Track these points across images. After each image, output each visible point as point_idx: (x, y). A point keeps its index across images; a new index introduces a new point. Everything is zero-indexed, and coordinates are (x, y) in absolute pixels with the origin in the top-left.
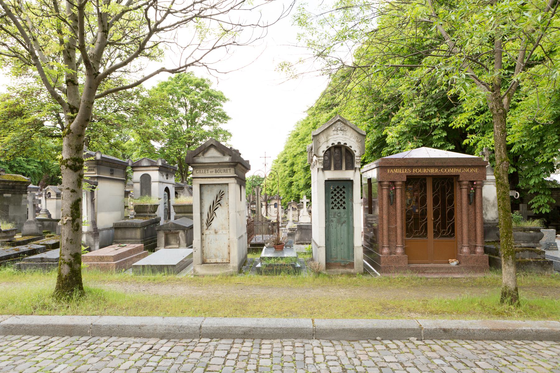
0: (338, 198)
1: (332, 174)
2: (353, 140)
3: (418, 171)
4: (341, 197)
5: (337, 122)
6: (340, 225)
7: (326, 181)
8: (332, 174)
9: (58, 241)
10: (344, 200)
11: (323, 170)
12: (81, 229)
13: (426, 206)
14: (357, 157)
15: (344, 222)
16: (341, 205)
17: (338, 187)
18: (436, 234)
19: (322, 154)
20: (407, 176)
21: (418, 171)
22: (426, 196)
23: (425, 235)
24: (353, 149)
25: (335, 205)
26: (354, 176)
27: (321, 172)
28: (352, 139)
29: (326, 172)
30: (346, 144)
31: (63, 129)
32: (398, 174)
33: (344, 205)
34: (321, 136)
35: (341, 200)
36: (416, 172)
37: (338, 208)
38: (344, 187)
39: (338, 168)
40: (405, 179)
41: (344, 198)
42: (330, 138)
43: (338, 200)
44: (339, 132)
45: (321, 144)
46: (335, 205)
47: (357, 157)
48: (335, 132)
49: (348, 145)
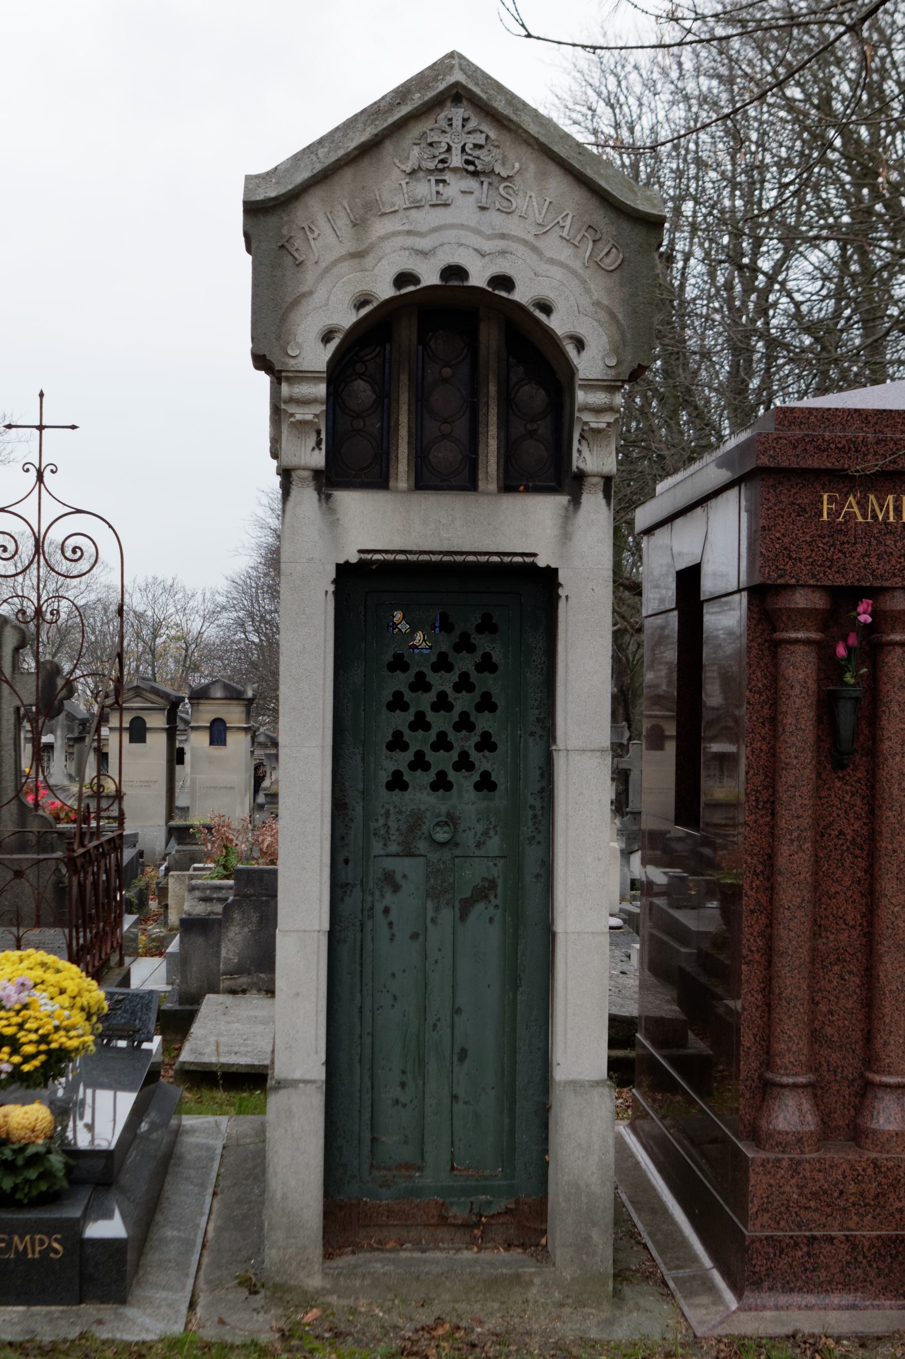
0: (442, 704)
1: (380, 523)
2: (565, 254)
4: (462, 702)
6: (447, 915)
10: (484, 722)
14: (591, 385)
15: (484, 892)
16: (464, 763)
28: (554, 247)
30: (404, 279)
33: (483, 762)
37: (441, 784)
38: (487, 626)
41: (487, 704)
42: (380, 227)
43: (440, 722)
44: (455, 185)
45: (310, 275)
46: (419, 763)
47: (591, 385)
48: (424, 189)
49: (522, 295)
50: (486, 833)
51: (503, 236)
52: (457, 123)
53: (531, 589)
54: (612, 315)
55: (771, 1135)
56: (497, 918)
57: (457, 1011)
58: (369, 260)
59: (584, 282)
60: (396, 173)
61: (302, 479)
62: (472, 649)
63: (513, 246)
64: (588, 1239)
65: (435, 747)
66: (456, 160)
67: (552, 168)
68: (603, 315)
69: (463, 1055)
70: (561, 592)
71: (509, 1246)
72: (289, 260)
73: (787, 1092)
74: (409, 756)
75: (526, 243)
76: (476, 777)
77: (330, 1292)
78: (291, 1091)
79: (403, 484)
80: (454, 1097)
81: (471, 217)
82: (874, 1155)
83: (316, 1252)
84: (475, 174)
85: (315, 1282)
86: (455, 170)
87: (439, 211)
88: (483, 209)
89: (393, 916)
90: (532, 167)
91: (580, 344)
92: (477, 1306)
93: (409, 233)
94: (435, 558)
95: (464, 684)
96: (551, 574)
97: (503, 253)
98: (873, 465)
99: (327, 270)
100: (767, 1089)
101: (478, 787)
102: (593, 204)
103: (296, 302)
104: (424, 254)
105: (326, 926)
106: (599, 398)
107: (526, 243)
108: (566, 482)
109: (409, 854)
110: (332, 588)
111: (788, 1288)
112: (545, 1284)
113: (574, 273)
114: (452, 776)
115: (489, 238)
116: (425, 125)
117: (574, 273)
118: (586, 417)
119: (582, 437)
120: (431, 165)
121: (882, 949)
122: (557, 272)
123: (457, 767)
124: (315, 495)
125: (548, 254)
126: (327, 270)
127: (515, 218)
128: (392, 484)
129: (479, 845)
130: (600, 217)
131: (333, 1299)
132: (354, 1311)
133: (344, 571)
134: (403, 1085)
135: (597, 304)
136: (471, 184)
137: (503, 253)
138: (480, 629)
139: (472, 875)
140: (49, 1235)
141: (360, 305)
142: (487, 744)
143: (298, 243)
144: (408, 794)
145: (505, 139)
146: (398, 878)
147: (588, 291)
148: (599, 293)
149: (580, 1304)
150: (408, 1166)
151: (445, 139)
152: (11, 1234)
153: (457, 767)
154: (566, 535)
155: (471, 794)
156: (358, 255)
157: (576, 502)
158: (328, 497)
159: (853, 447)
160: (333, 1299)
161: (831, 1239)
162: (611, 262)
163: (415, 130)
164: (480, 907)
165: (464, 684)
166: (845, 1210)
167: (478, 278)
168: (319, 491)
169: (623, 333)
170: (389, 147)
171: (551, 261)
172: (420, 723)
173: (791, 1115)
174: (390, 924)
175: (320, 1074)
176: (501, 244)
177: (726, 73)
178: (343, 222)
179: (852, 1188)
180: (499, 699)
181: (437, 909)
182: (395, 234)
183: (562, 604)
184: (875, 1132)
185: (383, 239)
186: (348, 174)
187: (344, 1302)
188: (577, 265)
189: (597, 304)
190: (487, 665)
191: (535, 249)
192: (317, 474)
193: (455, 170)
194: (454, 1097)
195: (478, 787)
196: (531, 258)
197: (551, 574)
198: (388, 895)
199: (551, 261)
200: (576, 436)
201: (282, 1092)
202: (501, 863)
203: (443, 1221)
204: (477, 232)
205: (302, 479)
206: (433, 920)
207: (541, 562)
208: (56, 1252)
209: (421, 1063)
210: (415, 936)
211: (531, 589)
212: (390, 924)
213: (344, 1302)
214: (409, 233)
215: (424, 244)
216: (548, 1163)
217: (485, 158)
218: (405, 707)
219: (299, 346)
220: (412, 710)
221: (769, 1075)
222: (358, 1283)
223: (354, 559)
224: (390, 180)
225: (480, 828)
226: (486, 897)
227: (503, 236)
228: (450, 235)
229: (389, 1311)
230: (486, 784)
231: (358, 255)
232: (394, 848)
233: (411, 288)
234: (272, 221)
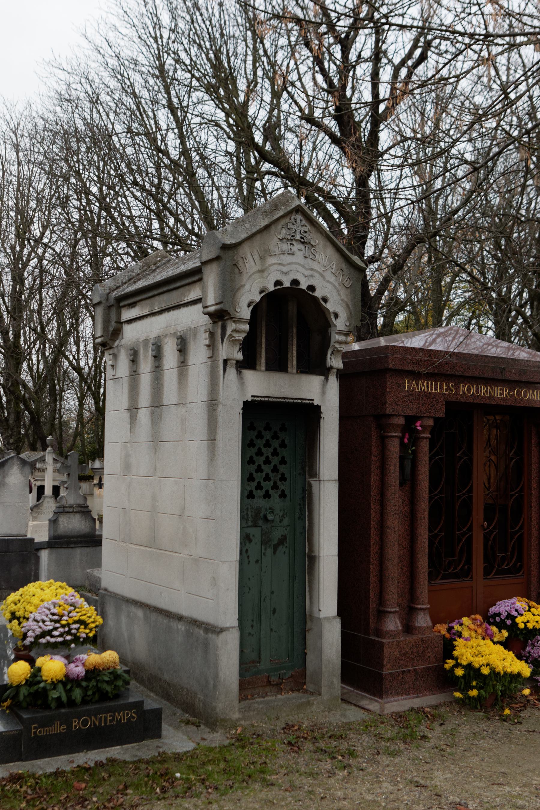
0: (267, 461)
1: (260, 384)
2: (332, 279)
3: (469, 390)
4: (275, 460)
5: (290, 213)
6: (269, 551)
7: (246, 403)
8: (260, 384)
9: (141, 699)
10: (282, 469)
11: (241, 366)
12: (316, 615)
13: (471, 491)
14: (340, 333)
15: (282, 541)
16: (275, 487)
17: (268, 428)
18: (487, 572)
19: (246, 313)
20: (448, 404)
21: (469, 390)
22: (471, 460)
23: (466, 573)
24: (330, 306)
25: (259, 487)
26: (323, 393)
27: (232, 371)
29: (248, 374)
30: (278, 283)
31: (519, 126)
32: (427, 395)
33: (282, 486)
34: (246, 249)
35: (275, 470)
36: (466, 391)
37: (267, 495)
38: (283, 429)
39: (277, 365)
40: (441, 414)
41: (283, 462)
42: (271, 261)
43: (267, 469)
44: (297, 246)
45: (245, 278)
46: (259, 487)
47: (340, 333)
48: (285, 246)
49: (318, 294)
50: (283, 516)
51: (312, 269)
52: (298, 221)
53: (310, 413)
54: (347, 305)
55: (388, 632)
56: (287, 551)
57: (272, 593)
58: (265, 274)
59: (338, 291)
60: (276, 239)
61: (232, 364)
62: (278, 438)
63: (316, 274)
64: (332, 683)
65: (265, 480)
66: (298, 237)
67: (328, 244)
68: (344, 305)
69: (274, 611)
70: (322, 416)
71: (292, 691)
72: (237, 271)
73: (391, 615)
74: (255, 484)
75: (319, 273)
76: (279, 493)
77: (242, 719)
78: (227, 632)
79: (263, 368)
80: (272, 630)
81: (302, 260)
82: (420, 636)
83: (236, 702)
84: (303, 243)
85: (236, 716)
86: (296, 240)
87: (290, 256)
88: (306, 257)
89: (249, 553)
90: (322, 243)
91: (336, 316)
92: (296, 717)
93: (280, 264)
94: (279, 400)
95: (275, 453)
96: (319, 407)
97: (312, 276)
98: (429, 369)
99: (250, 276)
100: (381, 614)
101: (280, 496)
102: (341, 260)
103: (239, 289)
104: (286, 273)
105: (238, 559)
106: (342, 338)
107: (319, 273)
108: (324, 371)
109: (255, 526)
110: (241, 412)
111: (397, 694)
112: (318, 703)
113: (335, 287)
114: (271, 492)
115: (307, 269)
116: (286, 220)
117: (335, 287)
118: (337, 345)
119: (332, 353)
120: (289, 237)
121: (419, 556)
122: (329, 286)
123: (272, 488)
124: (235, 371)
125: (327, 278)
126: (250, 276)
127: (316, 263)
128: (258, 367)
129: (281, 521)
130: (344, 266)
131: (243, 722)
132: (253, 726)
133: (246, 404)
134: (252, 626)
135: (343, 300)
136: (302, 247)
137: (312, 276)
138: (281, 430)
139: (277, 534)
140: (131, 710)
141: (261, 292)
142: (283, 478)
143: (241, 263)
144: (255, 500)
145: (313, 230)
146: (251, 537)
147: (340, 295)
148: (343, 297)
149: (330, 710)
150: (253, 662)
151: (294, 227)
152: (114, 712)
153: (272, 488)
154: (323, 393)
155: (278, 500)
156: (262, 271)
157: (327, 379)
158: (240, 372)
159: (418, 363)
160: (243, 722)
161: (409, 671)
162: (348, 284)
163: (283, 222)
164: (280, 547)
165: (275, 453)
166: (413, 659)
167: (303, 286)
168: (237, 369)
169: (351, 313)
170: (273, 227)
171: (328, 281)
172: (259, 470)
173: (393, 624)
174: (248, 557)
175: (236, 623)
176: (311, 272)
177: (171, 201)
178: (256, 257)
179: (415, 650)
180: (287, 459)
181: (265, 549)
182: (275, 264)
183: (322, 421)
184: (420, 627)
185: (271, 265)
186: (258, 237)
187: (247, 723)
188: (336, 284)
189: (343, 300)
190: (283, 445)
191: (323, 276)
192: (238, 362)
193: (296, 240)
194: (272, 630)
195: (280, 496)
196: (321, 279)
197: (319, 407)
198: (247, 544)
199: (328, 281)
200: (329, 352)
201: (224, 633)
202: (288, 529)
203: (269, 683)
204: (303, 267)
205: (232, 364)
206: (264, 554)
207: (316, 403)
208: (134, 718)
209: (260, 616)
210: (257, 562)
211: (310, 413)
212: (248, 557)
213: (247, 723)
214: (280, 264)
215: (285, 269)
216: (306, 654)
217: (308, 237)
218: (254, 463)
219: (240, 308)
220: (256, 464)
221: (381, 608)
222: (252, 713)
223: (250, 400)
224: (274, 241)
225: (281, 514)
226: (283, 544)
227: (312, 269)
228: (294, 267)
229: (266, 723)
230: (283, 495)
231: (262, 271)
232: (250, 524)
233: (279, 287)
234: (230, 253)
